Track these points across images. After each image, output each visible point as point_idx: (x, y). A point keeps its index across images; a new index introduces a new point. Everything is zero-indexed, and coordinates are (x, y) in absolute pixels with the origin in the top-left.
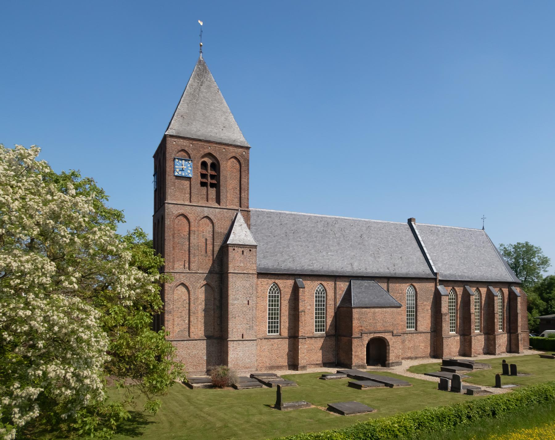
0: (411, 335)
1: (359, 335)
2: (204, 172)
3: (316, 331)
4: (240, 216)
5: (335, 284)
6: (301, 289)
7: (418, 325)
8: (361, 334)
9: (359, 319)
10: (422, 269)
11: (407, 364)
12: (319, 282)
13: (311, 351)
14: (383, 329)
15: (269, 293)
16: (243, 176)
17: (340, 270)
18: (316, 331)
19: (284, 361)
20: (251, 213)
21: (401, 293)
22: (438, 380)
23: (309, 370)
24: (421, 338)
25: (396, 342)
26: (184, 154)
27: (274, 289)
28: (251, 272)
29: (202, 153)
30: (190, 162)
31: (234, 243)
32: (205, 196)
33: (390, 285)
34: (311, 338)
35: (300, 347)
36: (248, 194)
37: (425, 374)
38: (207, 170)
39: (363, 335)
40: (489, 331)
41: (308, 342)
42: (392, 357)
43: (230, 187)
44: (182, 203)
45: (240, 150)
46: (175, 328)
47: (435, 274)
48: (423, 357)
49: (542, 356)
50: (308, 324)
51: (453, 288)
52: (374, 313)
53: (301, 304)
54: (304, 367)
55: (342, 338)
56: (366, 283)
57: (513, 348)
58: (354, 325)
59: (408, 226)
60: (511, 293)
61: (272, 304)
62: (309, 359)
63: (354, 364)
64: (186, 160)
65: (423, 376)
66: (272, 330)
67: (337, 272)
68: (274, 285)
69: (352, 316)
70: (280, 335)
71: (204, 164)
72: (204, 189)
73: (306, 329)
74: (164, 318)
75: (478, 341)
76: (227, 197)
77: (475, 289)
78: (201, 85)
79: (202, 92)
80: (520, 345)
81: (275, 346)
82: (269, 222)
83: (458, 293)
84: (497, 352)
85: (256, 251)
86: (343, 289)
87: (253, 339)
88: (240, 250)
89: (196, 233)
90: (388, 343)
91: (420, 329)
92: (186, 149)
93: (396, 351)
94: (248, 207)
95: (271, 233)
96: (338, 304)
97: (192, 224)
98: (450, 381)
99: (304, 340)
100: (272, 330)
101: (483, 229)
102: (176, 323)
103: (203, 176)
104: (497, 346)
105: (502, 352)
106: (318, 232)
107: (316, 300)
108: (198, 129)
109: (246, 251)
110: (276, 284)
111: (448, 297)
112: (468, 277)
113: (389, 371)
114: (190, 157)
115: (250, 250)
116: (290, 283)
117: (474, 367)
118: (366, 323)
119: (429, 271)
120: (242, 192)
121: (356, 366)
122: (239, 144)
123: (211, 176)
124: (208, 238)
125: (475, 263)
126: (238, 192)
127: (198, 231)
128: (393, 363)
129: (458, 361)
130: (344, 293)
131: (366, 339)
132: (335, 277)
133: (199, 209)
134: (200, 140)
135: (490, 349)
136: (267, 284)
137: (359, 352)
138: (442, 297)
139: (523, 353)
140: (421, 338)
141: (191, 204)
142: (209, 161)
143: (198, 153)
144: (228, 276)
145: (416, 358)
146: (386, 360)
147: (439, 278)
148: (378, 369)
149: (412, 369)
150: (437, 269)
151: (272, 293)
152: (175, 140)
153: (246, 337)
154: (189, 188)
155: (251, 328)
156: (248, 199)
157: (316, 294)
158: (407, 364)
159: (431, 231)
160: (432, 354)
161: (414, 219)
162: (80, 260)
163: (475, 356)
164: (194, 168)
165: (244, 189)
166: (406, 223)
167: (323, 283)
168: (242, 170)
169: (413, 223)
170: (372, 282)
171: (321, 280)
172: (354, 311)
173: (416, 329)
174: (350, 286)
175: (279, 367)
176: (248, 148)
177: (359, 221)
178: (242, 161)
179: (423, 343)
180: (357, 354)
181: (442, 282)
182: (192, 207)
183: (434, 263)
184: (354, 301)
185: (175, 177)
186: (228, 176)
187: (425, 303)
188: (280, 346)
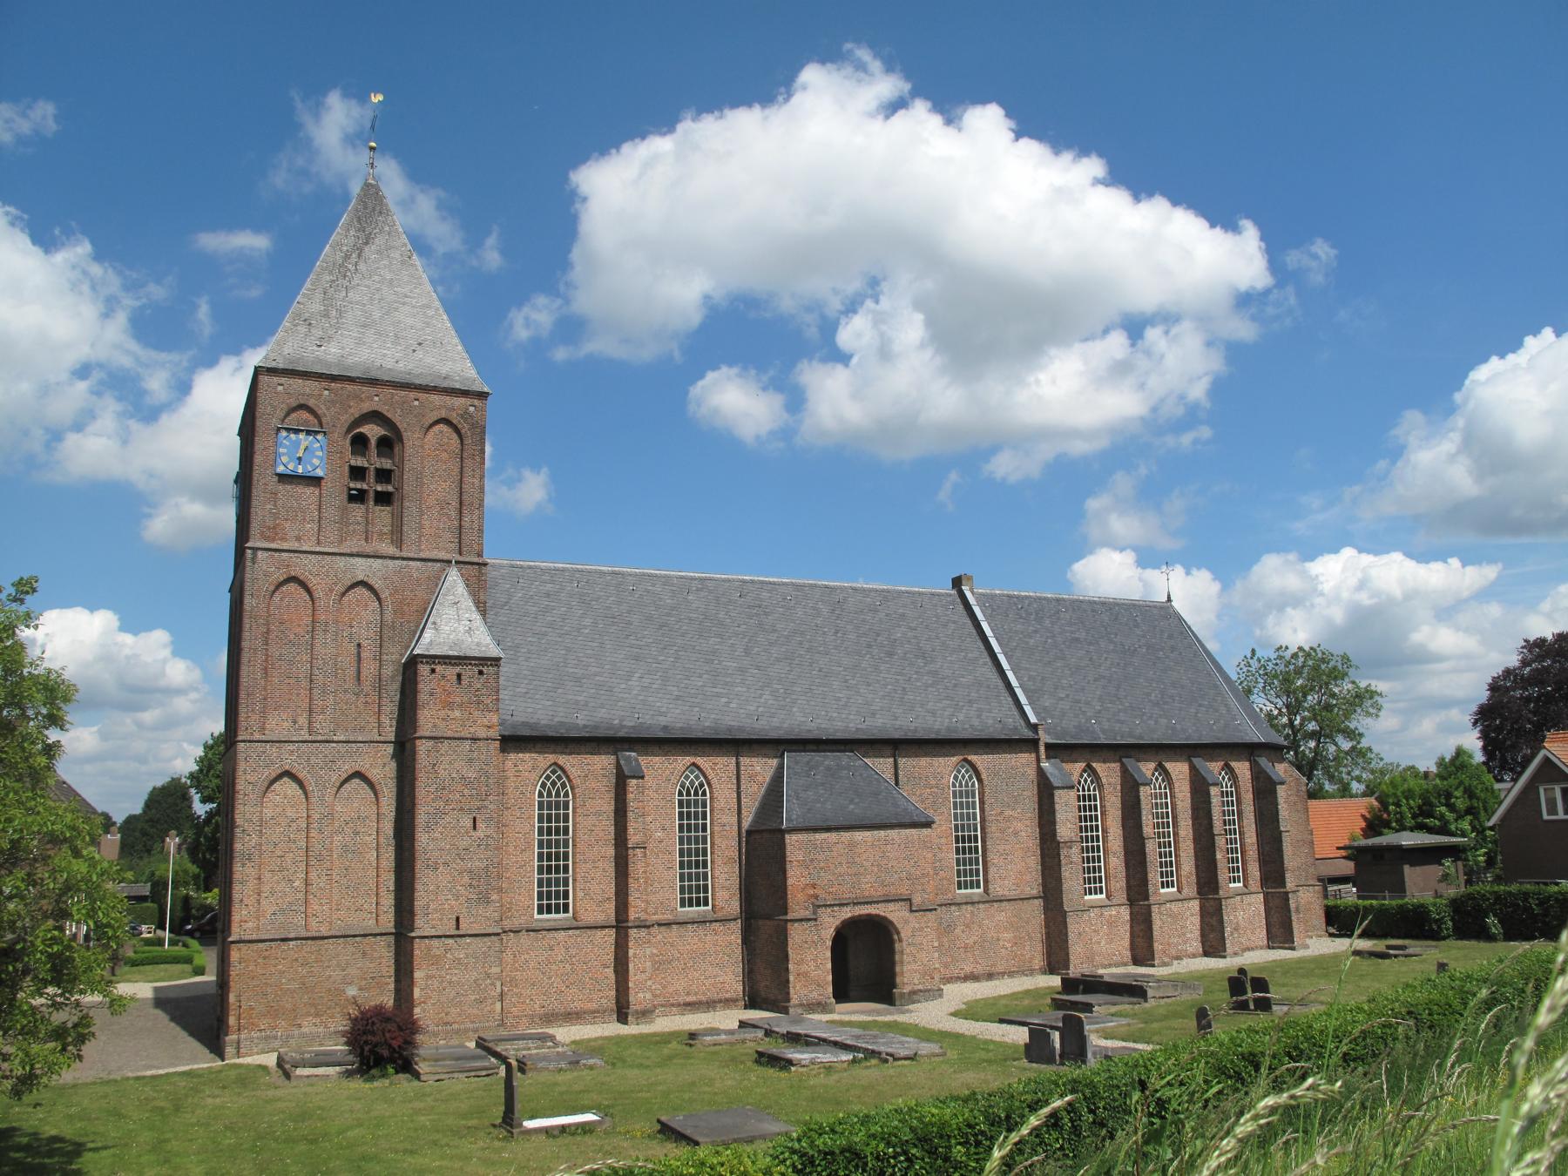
0: (969, 907)
2: (359, 462)
3: (683, 905)
6: (634, 782)
9: (804, 864)
11: (959, 993)
12: (689, 760)
15: (541, 795)
16: (468, 472)
18: (683, 905)
20: (491, 573)
22: (1020, 1035)
23: (664, 1024)
24: (1002, 914)
25: (921, 929)
26: (311, 418)
27: (554, 784)
28: (482, 733)
29: (356, 411)
30: (319, 437)
31: (432, 652)
33: (902, 761)
34: (668, 924)
35: (631, 952)
36: (481, 518)
37: (1002, 1021)
41: (659, 937)
42: (909, 973)
43: (431, 501)
44: (295, 546)
45: (460, 401)
46: (263, 902)
48: (1011, 974)
51: (1089, 766)
52: (852, 845)
54: (645, 1014)
55: (760, 922)
56: (829, 759)
58: (790, 882)
61: (549, 828)
62: (664, 987)
63: (795, 999)
64: (309, 433)
67: (740, 729)
68: (554, 772)
69: (784, 856)
72: (357, 511)
73: (652, 898)
74: (231, 872)
75: (1177, 917)
76: (421, 527)
77: (1152, 765)
78: (367, 243)
80: (1295, 925)
81: (560, 953)
83: (1104, 780)
86: (760, 778)
87: (490, 931)
88: (451, 672)
91: (998, 889)
92: (311, 403)
94: (480, 555)
96: (746, 824)
97: (321, 604)
98: (1057, 1034)
99: (643, 932)
100: (549, 906)
102: (266, 888)
103: (357, 473)
104: (1228, 930)
107: (681, 814)
109: (469, 672)
111: (1073, 793)
114: (321, 425)
115: (481, 673)
116: (602, 763)
117: (1150, 993)
118: (831, 872)
124: (364, 643)
125: (1149, 694)
127: (336, 622)
128: (914, 992)
129: (1106, 979)
130: (763, 790)
131: (830, 923)
132: (736, 745)
133: (341, 562)
136: (529, 767)
137: (810, 960)
138: (1057, 793)
139: (1306, 947)
140: (1002, 917)
142: (373, 431)
143: (341, 410)
144: (414, 746)
145: (990, 976)
146: (894, 985)
147: (1045, 738)
148: (857, 1012)
149: (970, 1012)
150: (1037, 714)
152: (283, 380)
155: (485, 899)
156: (481, 530)
157: (680, 794)
158: (959, 993)
163: (1165, 964)
165: (472, 504)
167: (700, 761)
170: (845, 758)
171: (696, 755)
172: (790, 839)
174: (781, 767)
176: (482, 396)
177: (812, 586)
178: (465, 428)
179: (1013, 929)
180: (804, 968)
181: (1054, 750)
182: (320, 557)
184: (790, 812)
187: (1008, 813)
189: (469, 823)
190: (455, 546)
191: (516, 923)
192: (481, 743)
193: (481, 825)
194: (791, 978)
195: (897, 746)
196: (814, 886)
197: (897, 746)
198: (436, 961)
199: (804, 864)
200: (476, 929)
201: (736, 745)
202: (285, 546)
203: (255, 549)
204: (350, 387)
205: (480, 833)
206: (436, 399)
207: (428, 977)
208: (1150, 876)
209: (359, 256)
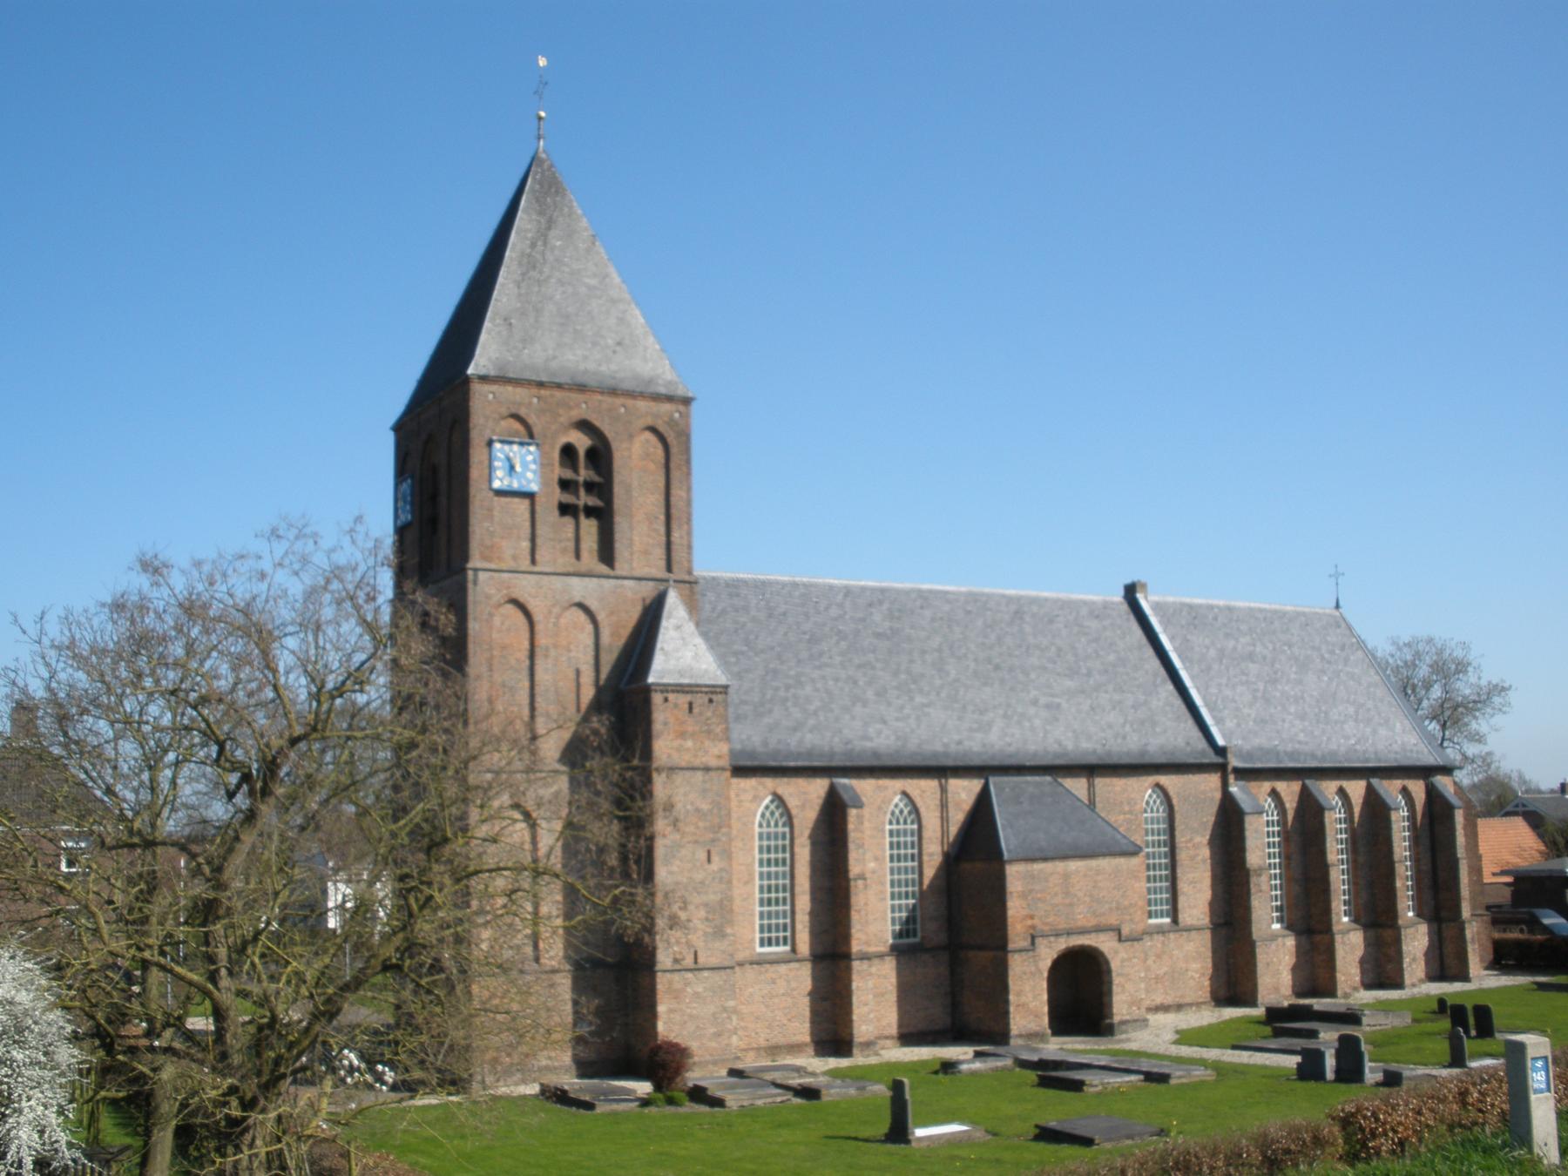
1: (1026, 944)
2: (568, 474)
4: (673, 600)
5: (943, 790)
7: (1180, 906)
8: (1033, 938)
9: (1023, 895)
10: (1177, 737)
13: (875, 998)
14: (1093, 922)
17: (953, 748)
19: (801, 1030)
21: (1130, 812)
25: (1129, 959)
27: (772, 814)
28: (713, 763)
30: (532, 448)
32: (571, 545)
35: (854, 985)
36: (689, 534)
37: (1235, 1047)
38: (575, 469)
39: (1038, 941)
40: (1378, 918)
42: (1121, 1006)
45: (666, 407)
47: (1221, 752)
49: (1542, 987)
50: (876, 917)
52: (1066, 876)
53: (853, 856)
55: (971, 954)
57: (1446, 963)
58: (1010, 913)
59: (1125, 607)
60: (1433, 795)
63: (1015, 1028)
64: (522, 444)
65: (1230, 1052)
66: (770, 939)
67: (946, 754)
70: (794, 950)
71: (568, 452)
72: (568, 521)
76: (631, 545)
79: (553, 249)
82: (737, 611)
84: (1408, 981)
85: (725, 701)
88: (683, 700)
89: (553, 653)
90: (1107, 962)
91: (1186, 917)
92: (523, 412)
93: (1129, 986)
94: (690, 572)
95: (747, 642)
97: (539, 628)
101: (1337, 606)
103: (565, 485)
104: (1406, 961)
105: (1418, 985)
106: (878, 635)
108: (576, 359)
110: (779, 799)
112: (1313, 756)
113: (1117, 1047)
114: (531, 436)
115: (711, 701)
116: (817, 789)
117: (1365, 1020)
118: (1047, 902)
119: (1202, 744)
120: (674, 526)
121: (1020, 1036)
122: (662, 390)
123: (589, 484)
126: (662, 529)
131: (1048, 953)
132: (940, 771)
133: (558, 582)
134: (559, 386)
135: (1382, 969)
137: (1028, 997)
141: (536, 569)
142: (582, 442)
145: (1179, 1007)
147: (1234, 762)
149: (1184, 1037)
150: (1224, 736)
151: (769, 825)
152: (494, 388)
153: (701, 960)
154: (527, 524)
156: (690, 547)
159: (1195, 617)
160: (1222, 993)
161: (1144, 586)
162: (489, 776)
164: (544, 465)
166: (1118, 597)
168: (672, 465)
169: (1140, 596)
173: (1175, 921)
175: (794, 1048)
176: (687, 401)
178: (671, 439)
179: (1192, 958)
180: (1023, 999)
181: (1245, 774)
183: (1214, 717)
185: (491, 494)
186: (635, 483)
188: (794, 985)
189: (703, 855)
190: (662, 563)
191: (740, 956)
192: (712, 774)
193: (715, 858)
194: (1012, 1009)
195: (1091, 770)
196: (1032, 917)
197: (1091, 770)
198: (677, 995)
199: (1023, 895)
200: (714, 961)
201: (940, 771)
202: (504, 566)
203: (476, 570)
204: (558, 394)
205: (715, 866)
206: (642, 405)
207: (671, 1011)
208: (1334, 905)
209: (545, 244)
